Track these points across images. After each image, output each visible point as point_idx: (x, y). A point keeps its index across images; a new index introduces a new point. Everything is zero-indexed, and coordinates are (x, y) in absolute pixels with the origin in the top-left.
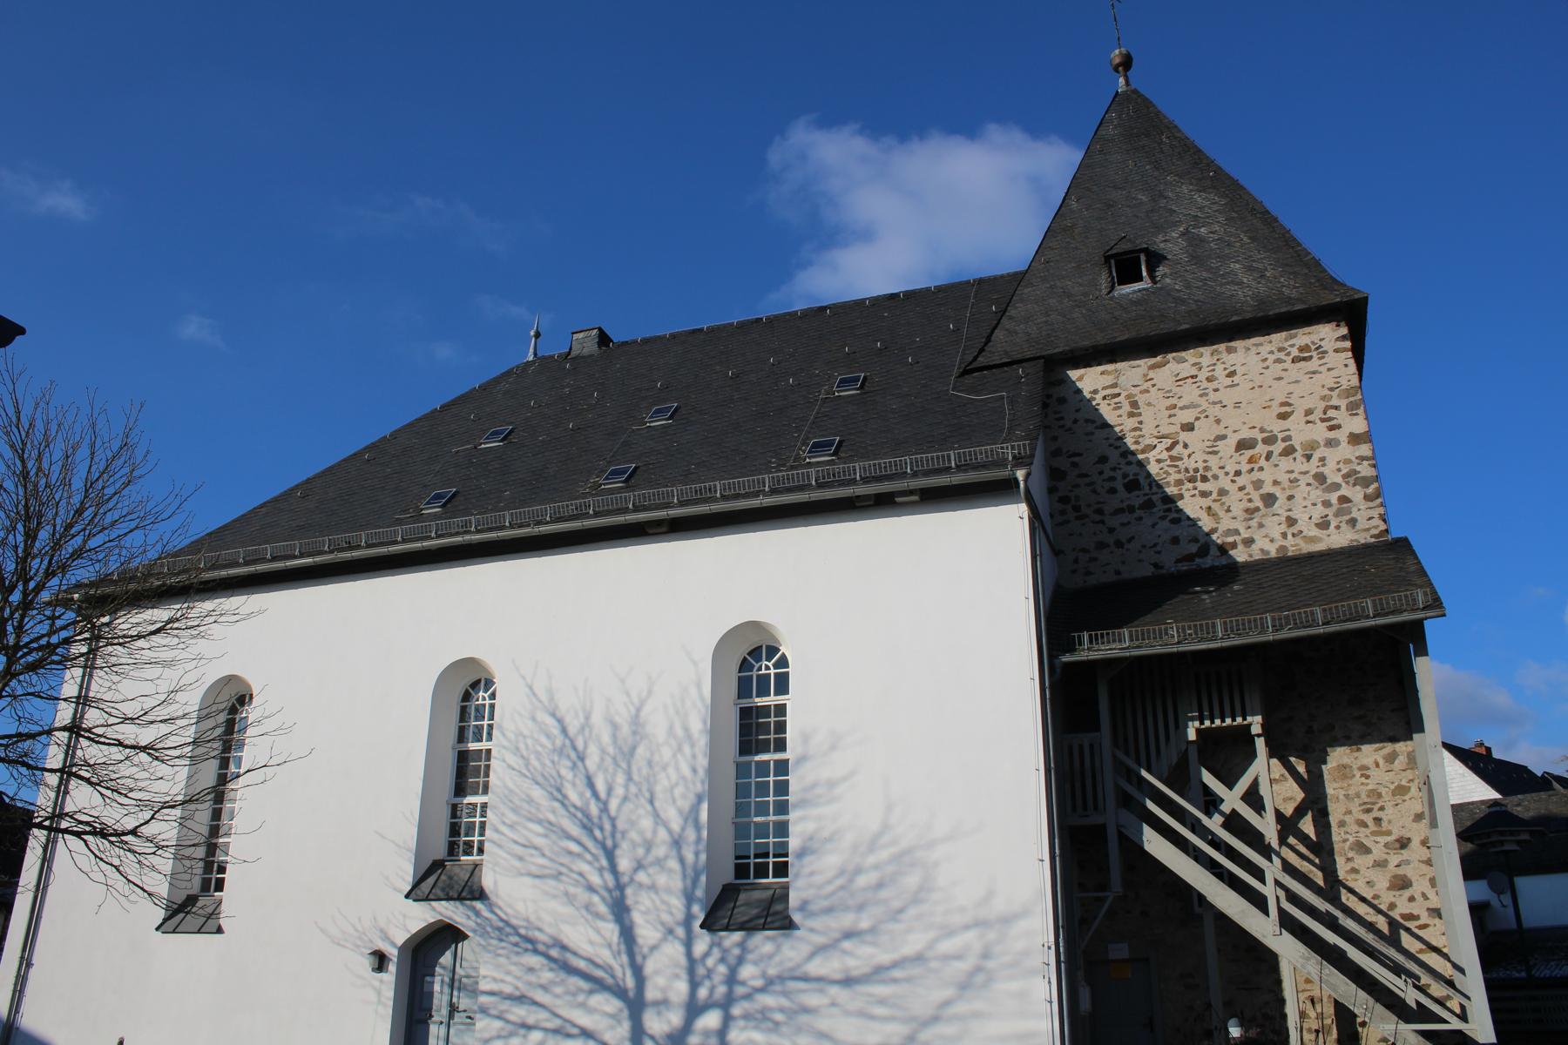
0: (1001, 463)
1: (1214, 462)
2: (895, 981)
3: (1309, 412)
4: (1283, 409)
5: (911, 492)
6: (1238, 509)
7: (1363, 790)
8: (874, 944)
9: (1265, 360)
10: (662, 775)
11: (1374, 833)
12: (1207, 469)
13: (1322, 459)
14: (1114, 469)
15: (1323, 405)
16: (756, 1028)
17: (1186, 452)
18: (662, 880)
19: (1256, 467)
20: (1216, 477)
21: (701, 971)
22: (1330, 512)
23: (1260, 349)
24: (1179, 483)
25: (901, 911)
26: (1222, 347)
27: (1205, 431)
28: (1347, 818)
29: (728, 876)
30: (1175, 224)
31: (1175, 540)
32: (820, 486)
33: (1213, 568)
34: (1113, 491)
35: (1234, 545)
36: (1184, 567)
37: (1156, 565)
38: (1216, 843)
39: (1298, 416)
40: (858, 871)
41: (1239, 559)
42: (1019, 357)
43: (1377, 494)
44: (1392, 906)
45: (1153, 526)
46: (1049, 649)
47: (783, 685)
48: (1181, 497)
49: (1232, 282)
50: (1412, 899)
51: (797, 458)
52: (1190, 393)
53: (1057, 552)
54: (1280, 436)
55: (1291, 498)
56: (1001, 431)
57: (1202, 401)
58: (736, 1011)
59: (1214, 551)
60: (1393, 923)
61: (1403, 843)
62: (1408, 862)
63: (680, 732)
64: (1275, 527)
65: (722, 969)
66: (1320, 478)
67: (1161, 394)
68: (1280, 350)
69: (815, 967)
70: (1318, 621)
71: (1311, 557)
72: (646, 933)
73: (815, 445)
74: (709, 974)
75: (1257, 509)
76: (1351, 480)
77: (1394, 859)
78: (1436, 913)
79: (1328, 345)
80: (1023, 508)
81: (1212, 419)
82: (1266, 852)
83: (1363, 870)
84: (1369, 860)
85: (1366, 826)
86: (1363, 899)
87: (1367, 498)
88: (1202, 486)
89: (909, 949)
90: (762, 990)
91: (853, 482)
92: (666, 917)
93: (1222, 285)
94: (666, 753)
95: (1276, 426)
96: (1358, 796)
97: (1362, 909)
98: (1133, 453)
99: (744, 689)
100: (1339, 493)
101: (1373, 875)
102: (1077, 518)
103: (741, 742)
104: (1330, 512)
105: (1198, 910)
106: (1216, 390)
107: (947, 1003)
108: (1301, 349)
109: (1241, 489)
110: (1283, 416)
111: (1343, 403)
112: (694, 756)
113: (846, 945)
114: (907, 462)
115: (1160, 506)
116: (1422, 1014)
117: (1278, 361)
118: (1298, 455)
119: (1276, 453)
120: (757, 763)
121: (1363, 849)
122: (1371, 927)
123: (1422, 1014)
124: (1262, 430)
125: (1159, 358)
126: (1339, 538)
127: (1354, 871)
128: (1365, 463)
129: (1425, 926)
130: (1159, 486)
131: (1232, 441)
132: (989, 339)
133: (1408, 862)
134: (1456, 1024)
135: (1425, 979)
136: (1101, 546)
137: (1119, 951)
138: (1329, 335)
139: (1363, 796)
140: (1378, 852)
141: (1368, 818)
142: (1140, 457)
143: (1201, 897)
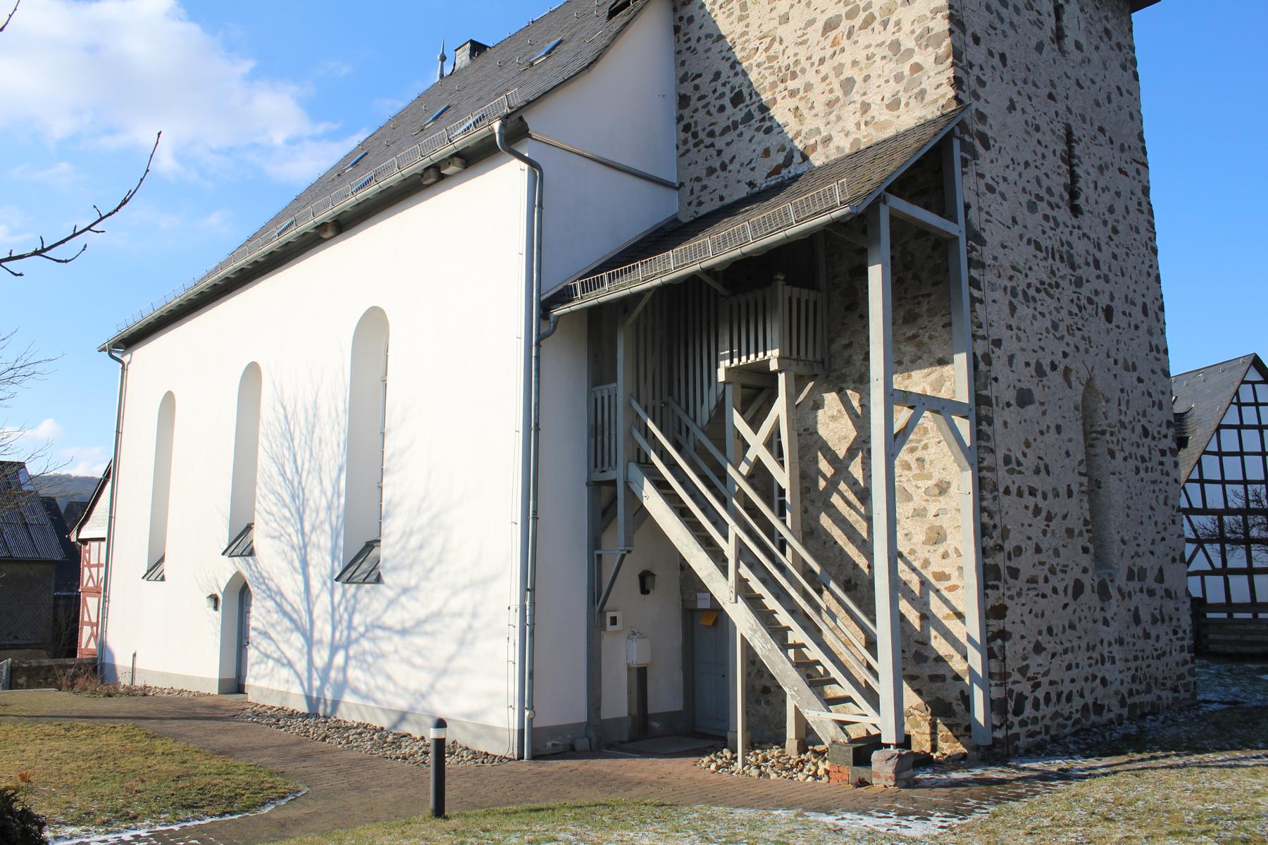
8: (416, 599)
11: (916, 477)
12: (797, 62)
19: (838, 48)
22: (901, 87)
24: (773, 85)
35: (814, 148)
40: (411, 534)
44: (926, 563)
50: (945, 555)
55: (867, 78)
60: (924, 582)
62: (945, 511)
64: (850, 117)
66: (895, 46)
69: (392, 619)
72: (316, 585)
75: (838, 99)
88: (791, 85)
100: (912, 61)
107: (451, 658)
113: (403, 599)
115: (758, 115)
119: (857, 28)
129: (952, 588)
133: (945, 511)
136: (711, 171)
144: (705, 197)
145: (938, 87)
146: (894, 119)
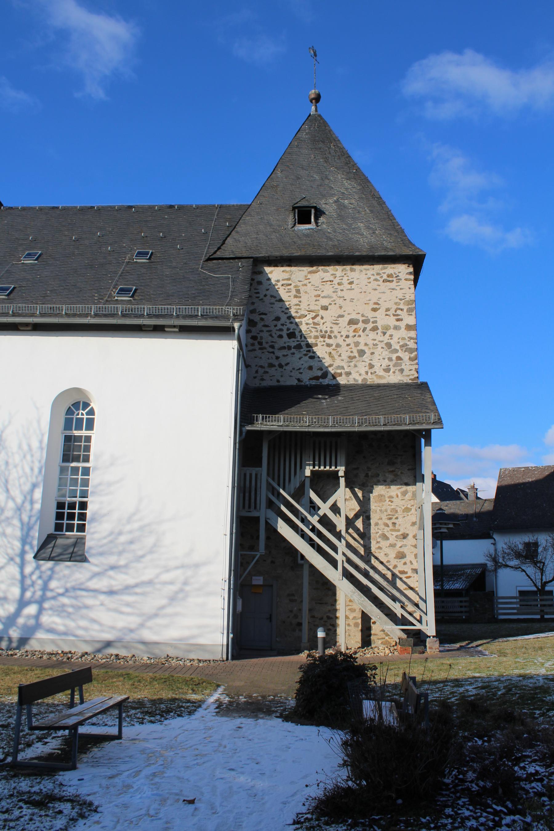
0: (226, 318)
1: (336, 329)
2: (136, 594)
3: (388, 310)
4: (375, 306)
5: (174, 327)
6: (345, 356)
7: (389, 508)
8: (126, 573)
9: (370, 278)
10: (14, 470)
11: (391, 530)
13: (391, 336)
14: (283, 325)
15: (395, 307)
16: (58, 615)
17: (322, 321)
18: (9, 530)
19: (357, 334)
20: (336, 337)
21: (28, 582)
22: (392, 364)
23: (368, 272)
24: (316, 337)
25: (143, 556)
26: (348, 267)
27: (333, 311)
28: (380, 522)
29: (51, 529)
30: (333, 195)
31: (311, 368)
32: (124, 316)
33: (328, 385)
34: (281, 336)
35: (340, 375)
36: (314, 382)
37: (299, 380)
38: (313, 529)
39: (382, 311)
40: (120, 533)
41: (341, 383)
42: (240, 255)
43: (416, 358)
45: (300, 359)
46: (241, 422)
47: (90, 425)
48: (316, 345)
49: (358, 233)
50: (405, 564)
51: (110, 296)
52: (328, 290)
53: (247, 366)
54: (372, 320)
55: (372, 353)
56: (227, 297)
57: (334, 295)
58: (46, 605)
59: (330, 377)
60: (394, 575)
61: (405, 536)
62: (406, 546)
63: (25, 447)
64: (362, 368)
65: (40, 582)
66: (389, 345)
67: (313, 288)
68: (378, 274)
69: (94, 584)
70: (380, 423)
71: (379, 386)
73: (121, 290)
74: (33, 584)
75: (355, 357)
76: (404, 349)
77: (399, 544)
78: (416, 571)
79: (403, 276)
80: (235, 343)
81: (338, 305)
82: (339, 536)
83: (384, 548)
84: (387, 543)
85: (388, 526)
86: (382, 563)
87: (410, 359)
88: (328, 341)
89: (145, 577)
90: (62, 595)
91: (142, 316)
92: (10, 551)
93: (352, 234)
94: (17, 458)
95: (371, 315)
96: (386, 511)
97: (380, 567)
98: (293, 318)
99: (68, 425)
101: (387, 550)
102: (260, 349)
103: (64, 455)
104: (392, 364)
105: (300, 562)
106: (342, 290)
107: (163, 607)
108: (388, 276)
109: (348, 345)
110: (374, 310)
111: (405, 308)
112: (33, 462)
113: (111, 573)
114: (174, 309)
115: (305, 348)
116: (403, 621)
117: (376, 280)
118: (379, 331)
119: (368, 329)
120: (72, 467)
121: (385, 537)
122: (383, 576)
123: (403, 621)
124: (363, 316)
125: (314, 268)
126: (394, 378)
127: (380, 548)
128: (412, 341)
130: (305, 338)
131: (347, 319)
132: (224, 243)
133: (406, 546)
134: (418, 626)
135: (406, 602)
136: (271, 365)
137: (258, 580)
138: (404, 270)
139: (389, 511)
140: (392, 540)
141: (390, 523)
142: (297, 320)
143: (303, 557)
144: (266, 377)
145: (410, 370)
146: (387, 376)
